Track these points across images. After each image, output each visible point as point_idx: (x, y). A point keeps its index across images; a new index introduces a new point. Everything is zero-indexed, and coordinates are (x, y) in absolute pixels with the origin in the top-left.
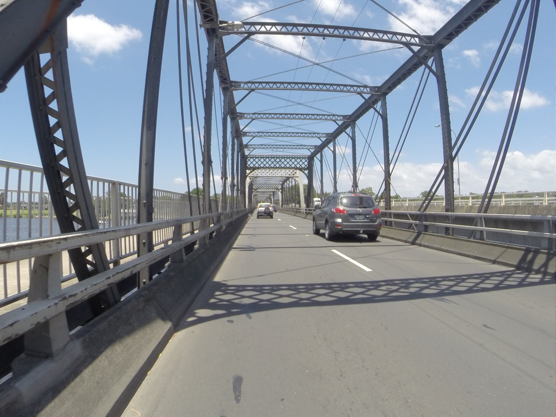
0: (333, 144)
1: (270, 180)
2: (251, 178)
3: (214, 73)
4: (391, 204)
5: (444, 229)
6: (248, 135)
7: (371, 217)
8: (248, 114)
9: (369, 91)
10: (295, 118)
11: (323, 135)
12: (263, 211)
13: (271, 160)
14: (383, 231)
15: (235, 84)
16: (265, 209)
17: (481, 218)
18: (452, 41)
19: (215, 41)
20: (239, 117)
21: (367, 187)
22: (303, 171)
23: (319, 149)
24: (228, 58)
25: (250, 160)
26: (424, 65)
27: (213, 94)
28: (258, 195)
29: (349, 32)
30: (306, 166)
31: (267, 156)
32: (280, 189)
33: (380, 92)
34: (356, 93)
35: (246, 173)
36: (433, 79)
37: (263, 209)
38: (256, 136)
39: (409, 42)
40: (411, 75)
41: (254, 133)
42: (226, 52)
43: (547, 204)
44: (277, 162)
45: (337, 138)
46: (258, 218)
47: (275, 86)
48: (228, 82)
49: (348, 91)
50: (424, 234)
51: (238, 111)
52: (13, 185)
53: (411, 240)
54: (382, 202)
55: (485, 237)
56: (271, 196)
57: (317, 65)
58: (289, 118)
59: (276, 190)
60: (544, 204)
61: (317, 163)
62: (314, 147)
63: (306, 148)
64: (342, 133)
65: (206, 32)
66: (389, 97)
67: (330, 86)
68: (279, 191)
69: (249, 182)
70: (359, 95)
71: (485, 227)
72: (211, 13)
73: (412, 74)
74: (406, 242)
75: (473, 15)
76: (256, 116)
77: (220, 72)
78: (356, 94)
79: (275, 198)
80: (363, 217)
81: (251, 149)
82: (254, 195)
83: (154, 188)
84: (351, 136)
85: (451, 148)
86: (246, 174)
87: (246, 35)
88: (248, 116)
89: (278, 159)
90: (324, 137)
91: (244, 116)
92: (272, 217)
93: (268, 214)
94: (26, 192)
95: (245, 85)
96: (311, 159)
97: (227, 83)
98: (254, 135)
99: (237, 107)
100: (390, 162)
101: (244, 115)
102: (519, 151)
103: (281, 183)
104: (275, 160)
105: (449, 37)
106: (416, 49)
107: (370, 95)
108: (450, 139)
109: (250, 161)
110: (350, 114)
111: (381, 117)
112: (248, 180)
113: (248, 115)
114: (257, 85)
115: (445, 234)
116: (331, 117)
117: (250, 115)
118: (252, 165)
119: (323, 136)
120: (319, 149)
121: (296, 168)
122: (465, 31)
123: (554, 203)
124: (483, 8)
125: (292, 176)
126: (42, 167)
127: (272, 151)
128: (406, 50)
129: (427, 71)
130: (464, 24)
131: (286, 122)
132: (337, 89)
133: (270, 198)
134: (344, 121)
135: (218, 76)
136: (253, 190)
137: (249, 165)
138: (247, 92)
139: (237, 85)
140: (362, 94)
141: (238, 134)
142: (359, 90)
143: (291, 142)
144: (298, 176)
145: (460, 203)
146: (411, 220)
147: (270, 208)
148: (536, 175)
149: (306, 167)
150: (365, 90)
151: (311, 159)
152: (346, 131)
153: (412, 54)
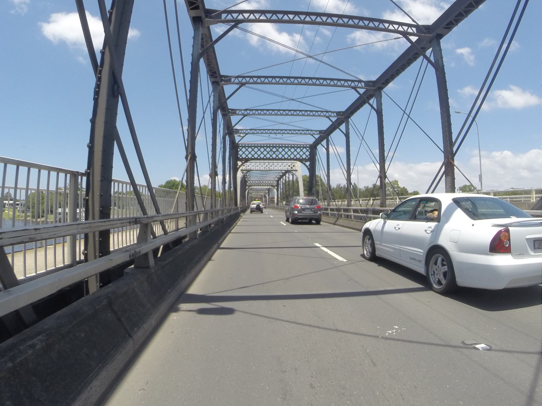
1: (264, 178)
2: (243, 171)
4: (386, 202)
6: (241, 133)
7: (315, 210)
8: (240, 110)
9: (364, 86)
10: (288, 114)
11: (316, 132)
14: (323, 218)
16: (257, 206)
18: (451, 30)
19: (201, 31)
20: (230, 114)
21: (393, 180)
22: (304, 162)
23: (325, 135)
24: (216, 46)
25: (242, 150)
26: (423, 56)
27: (199, 76)
28: (253, 193)
30: (307, 156)
31: (262, 145)
33: (374, 87)
35: (237, 164)
36: (431, 70)
38: (249, 133)
39: (406, 32)
40: (417, 60)
41: (247, 130)
43: (534, 200)
44: (273, 152)
45: (331, 135)
46: (251, 213)
47: (262, 113)
48: (218, 77)
51: (229, 107)
52: (10, 182)
54: (371, 200)
56: (266, 194)
57: (310, 57)
58: (281, 115)
59: (271, 187)
60: (532, 201)
61: (321, 150)
62: (335, 114)
63: (309, 134)
65: (192, 21)
66: (445, 43)
67: (304, 112)
68: (275, 188)
69: (241, 176)
71: (373, 215)
76: (246, 113)
77: (208, 59)
79: (271, 196)
80: (310, 210)
81: (242, 135)
82: (250, 196)
83: (113, 178)
84: (376, 107)
85: (452, 144)
86: (237, 167)
87: (233, 24)
89: (274, 148)
91: (236, 112)
92: (262, 212)
93: (259, 209)
94: (23, 189)
95: (235, 79)
96: (313, 148)
97: (216, 77)
98: (247, 132)
99: (228, 102)
100: (385, 158)
101: (236, 111)
102: (508, 151)
103: (277, 179)
104: (271, 150)
105: (447, 26)
106: (414, 39)
107: (365, 90)
108: (450, 133)
110: (344, 110)
111: (376, 111)
112: (239, 175)
114: (248, 79)
116: (325, 113)
117: (242, 111)
118: (244, 156)
119: (316, 133)
120: (325, 135)
121: (297, 159)
123: (528, 200)
125: (290, 168)
126: (130, 182)
127: (268, 138)
129: (425, 61)
130: (465, 11)
131: (280, 119)
132: (331, 84)
133: (265, 197)
134: (338, 118)
137: (241, 156)
138: (238, 86)
139: (228, 80)
140: (357, 89)
141: (230, 131)
142: (353, 85)
143: (291, 124)
144: (297, 169)
148: (525, 173)
149: (307, 158)
150: (360, 85)
151: (313, 148)
152: (340, 128)
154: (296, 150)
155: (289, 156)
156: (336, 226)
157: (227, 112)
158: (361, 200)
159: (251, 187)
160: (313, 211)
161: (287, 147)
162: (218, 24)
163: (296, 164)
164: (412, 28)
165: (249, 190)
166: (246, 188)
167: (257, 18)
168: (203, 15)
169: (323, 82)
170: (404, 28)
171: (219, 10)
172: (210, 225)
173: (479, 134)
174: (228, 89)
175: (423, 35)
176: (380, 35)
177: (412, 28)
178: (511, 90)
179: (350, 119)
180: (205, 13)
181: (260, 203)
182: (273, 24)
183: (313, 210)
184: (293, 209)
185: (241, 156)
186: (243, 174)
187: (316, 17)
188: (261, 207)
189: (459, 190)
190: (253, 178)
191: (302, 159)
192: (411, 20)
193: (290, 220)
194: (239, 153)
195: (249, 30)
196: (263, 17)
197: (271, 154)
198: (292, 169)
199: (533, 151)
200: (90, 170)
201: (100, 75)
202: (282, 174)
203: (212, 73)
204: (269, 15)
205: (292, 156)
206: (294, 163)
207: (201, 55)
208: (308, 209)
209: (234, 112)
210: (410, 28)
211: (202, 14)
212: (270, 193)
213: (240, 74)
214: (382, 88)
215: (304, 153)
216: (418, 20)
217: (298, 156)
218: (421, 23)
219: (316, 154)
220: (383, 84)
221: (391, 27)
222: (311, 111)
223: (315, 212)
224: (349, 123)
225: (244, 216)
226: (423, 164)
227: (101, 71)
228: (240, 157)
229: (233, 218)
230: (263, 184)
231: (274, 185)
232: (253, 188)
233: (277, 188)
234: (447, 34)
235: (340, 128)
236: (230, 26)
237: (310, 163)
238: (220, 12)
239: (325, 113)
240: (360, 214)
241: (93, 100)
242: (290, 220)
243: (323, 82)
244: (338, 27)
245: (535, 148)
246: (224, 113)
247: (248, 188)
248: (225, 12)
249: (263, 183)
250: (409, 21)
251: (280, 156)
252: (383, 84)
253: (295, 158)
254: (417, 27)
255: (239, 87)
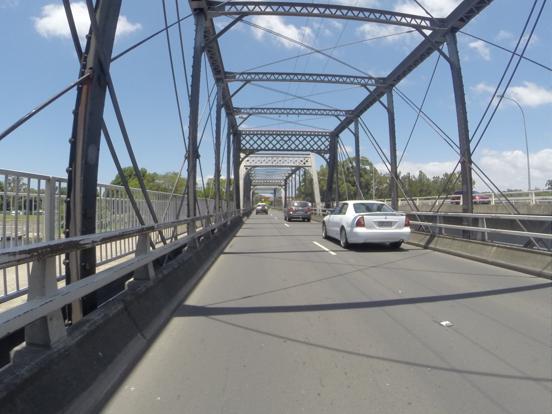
0: (354, 125)
2: (247, 167)
3: (202, 57)
5: (462, 232)
6: (243, 112)
8: (246, 109)
9: (374, 83)
12: (261, 209)
13: (277, 139)
15: (230, 76)
17: (482, 219)
29: (352, 13)
30: (326, 147)
32: (283, 186)
33: (385, 84)
34: (360, 85)
35: (240, 157)
37: (260, 208)
38: (254, 114)
40: (417, 67)
42: (217, 33)
44: (285, 141)
46: (257, 214)
49: (352, 83)
50: (439, 237)
51: (234, 106)
53: (423, 244)
55: (487, 238)
57: (318, 52)
59: (278, 187)
62: (344, 113)
64: (344, 129)
69: (245, 173)
70: (363, 87)
71: (487, 228)
72: (219, 67)
73: (406, 75)
74: (417, 245)
75: (475, 7)
78: (361, 86)
81: (245, 116)
85: (468, 141)
86: (240, 160)
87: (237, 16)
88: (245, 111)
90: (343, 115)
91: (241, 111)
92: (267, 214)
95: (240, 76)
96: (334, 136)
99: (233, 99)
102: (519, 150)
103: (285, 178)
104: (282, 139)
106: (428, 32)
107: (376, 87)
108: (467, 131)
109: (245, 140)
112: (242, 171)
113: (245, 110)
114: (253, 76)
115: (463, 236)
118: (248, 146)
121: (313, 151)
122: (428, 58)
124: (425, 54)
125: (302, 164)
128: (416, 33)
135: (209, 62)
136: (252, 187)
137: (244, 146)
139: (231, 76)
140: (367, 86)
141: (233, 126)
142: (363, 82)
145: (528, 201)
146: (420, 221)
147: (266, 207)
149: (326, 149)
150: (370, 82)
151: (334, 136)
152: (349, 127)
153: (423, 39)
154: (312, 139)
155: (304, 146)
156: (428, 251)
157: (231, 112)
158: (400, 200)
159: (256, 187)
160: (304, 212)
161: (302, 135)
162: (222, 16)
163: (309, 159)
164: (426, 21)
165: (255, 190)
166: (251, 188)
167: (263, 10)
168: (223, 76)
169: (332, 79)
170: (417, 21)
171: (222, 1)
172: (213, 231)
173: (526, 122)
174: (233, 86)
175: (437, 28)
176: (392, 28)
177: (426, 21)
178: (525, 86)
179: (359, 118)
180: (208, 5)
181: (265, 205)
182: (280, 16)
183: (304, 211)
184: (289, 211)
185: (244, 146)
186: (246, 171)
187: (324, 9)
188: (266, 209)
189: (547, 185)
190: (258, 176)
191: (320, 150)
192: (425, 12)
193: (287, 219)
194: (242, 142)
195: (253, 22)
196: (269, 10)
197: (282, 144)
198: (305, 165)
199: (545, 150)
200: (72, 168)
201: (84, 63)
202: (288, 175)
203: (213, 61)
204: (275, 8)
205: (308, 147)
206: (307, 158)
207: (203, 50)
208: (300, 210)
209: (238, 111)
210: (423, 21)
211: (223, 76)
212: (276, 193)
213: (244, 71)
214: (393, 86)
215: (323, 143)
216: (432, 10)
217: (315, 147)
218: (435, 15)
219: (338, 142)
220: (394, 80)
221: (403, 20)
222: (319, 110)
223: (306, 212)
224: (359, 123)
225: (248, 220)
226: (432, 163)
227: (86, 58)
228: (243, 147)
229: (237, 223)
230: (269, 183)
231: (282, 184)
232: (258, 188)
233: (285, 188)
234: (462, 28)
235: (349, 127)
236: (234, 19)
237: (330, 155)
238: (223, 3)
239: (334, 112)
240: (420, 223)
241: (77, 90)
242: (287, 219)
243: (332, 79)
244: (349, 20)
245: (547, 148)
246: (219, 76)
247: (253, 188)
248: (228, 4)
249: (269, 182)
250: (423, 14)
251: (293, 146)
252: (394, 80)
253: (312, 149)
254: (432, 20)
255: (244, 84)
